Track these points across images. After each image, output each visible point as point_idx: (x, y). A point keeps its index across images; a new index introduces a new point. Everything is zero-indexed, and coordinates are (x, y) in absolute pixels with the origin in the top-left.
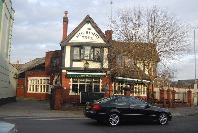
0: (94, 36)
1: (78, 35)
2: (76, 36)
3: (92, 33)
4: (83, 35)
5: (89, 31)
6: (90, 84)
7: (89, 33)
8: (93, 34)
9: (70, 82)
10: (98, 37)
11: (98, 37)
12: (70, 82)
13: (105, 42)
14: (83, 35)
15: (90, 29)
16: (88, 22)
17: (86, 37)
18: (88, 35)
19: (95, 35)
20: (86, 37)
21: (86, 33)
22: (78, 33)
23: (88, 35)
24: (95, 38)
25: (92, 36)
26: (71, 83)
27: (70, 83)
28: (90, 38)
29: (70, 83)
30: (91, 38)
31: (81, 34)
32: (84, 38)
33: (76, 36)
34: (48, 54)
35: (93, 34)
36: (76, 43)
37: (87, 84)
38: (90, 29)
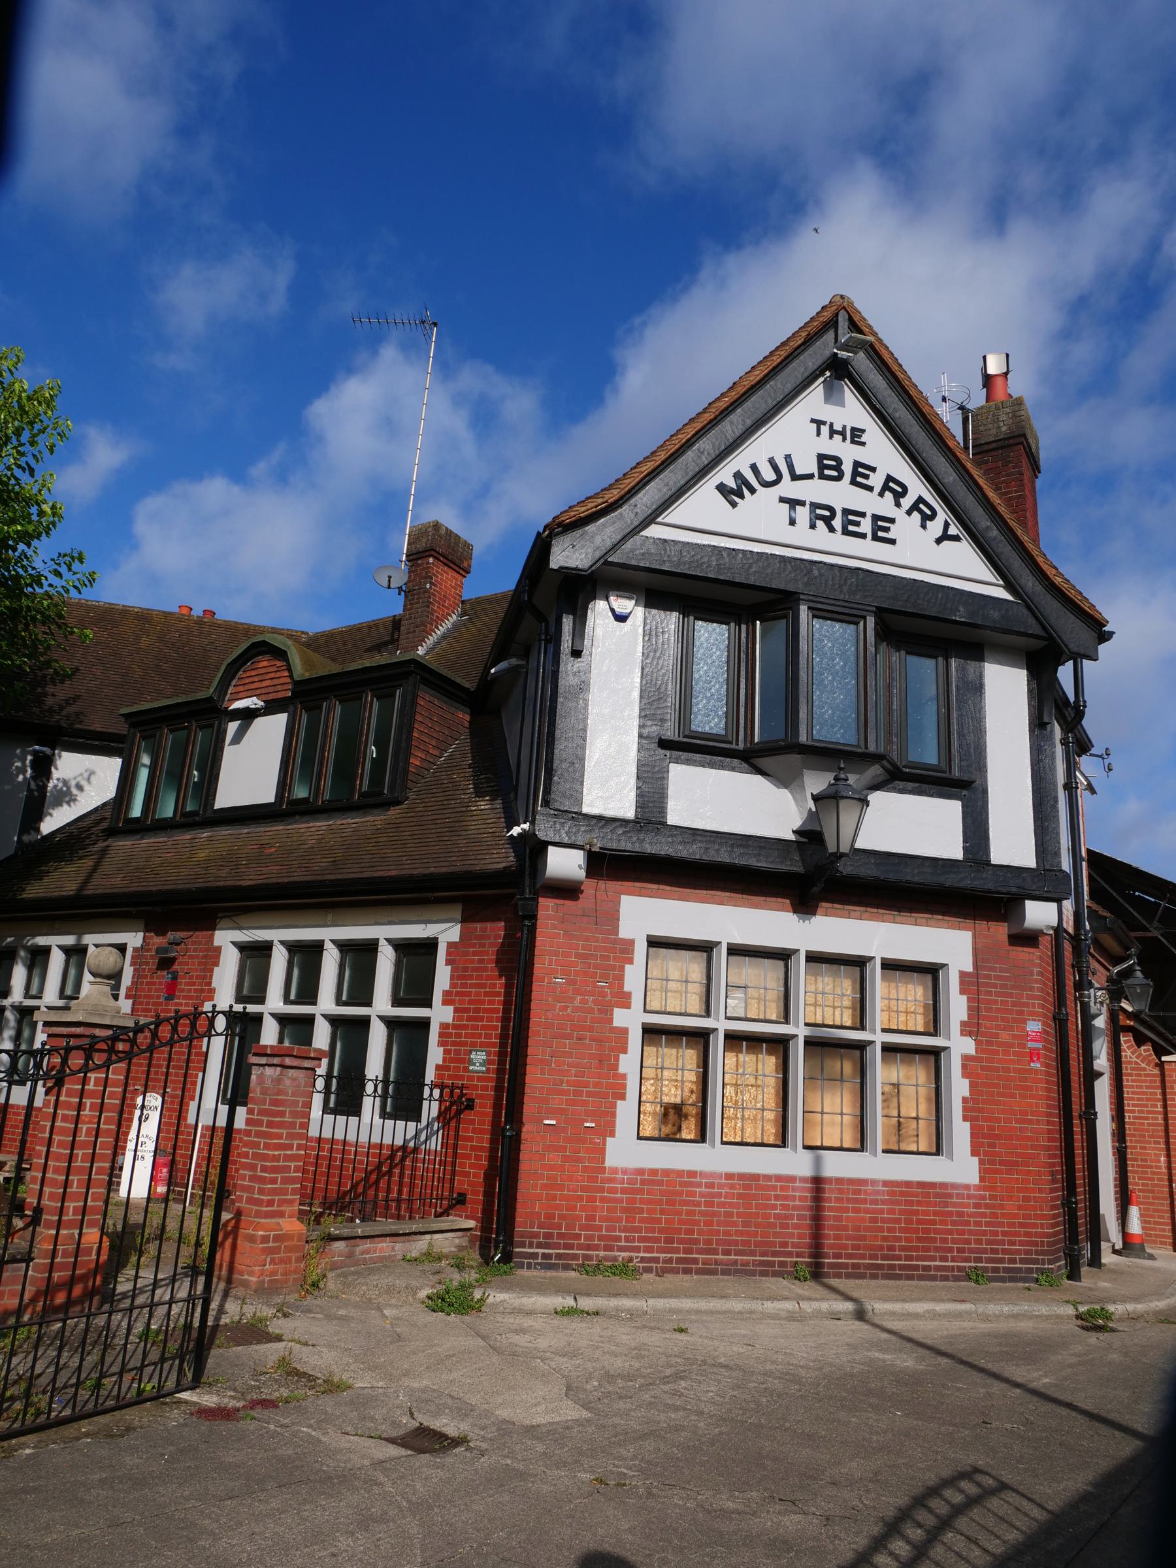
0: (899, 514)
1: (738, 475)
2: (722, 488)
3: (876, 481)
4: (788, 488)
5: (849, 454)
6: (389, 1100)
7: (847, 468)
8: (886, 487)
9: (624, 1000)
10: (936, 528)
11: (936, 528)
12: (624, 1000)
13: (1009, 586)
14: (788, 488)
15: (856, 436)
16: (838, 370)
17: (823, 515)
18: (840, 495)
19: (907, 502)
20: (823, 515)
21: (822, 467)
22: (740, 462)
23: (840, 495)
24: (906, 526)
25: (885, 506)
26: (139, 1087)
27: (620, 1018)
28: (866, 526)
29: (620, 1018)
30: (876, 529)
31: (769, 475)
32: (803, 513)
33: (722, 488)
34: (974, 1153)
35: (894, 488)
36: (722, 767)
37: (369, 1105)
38: (856, 436)
